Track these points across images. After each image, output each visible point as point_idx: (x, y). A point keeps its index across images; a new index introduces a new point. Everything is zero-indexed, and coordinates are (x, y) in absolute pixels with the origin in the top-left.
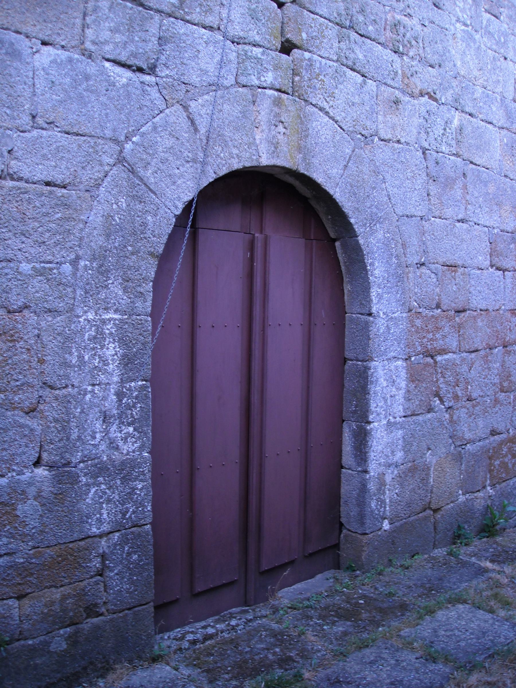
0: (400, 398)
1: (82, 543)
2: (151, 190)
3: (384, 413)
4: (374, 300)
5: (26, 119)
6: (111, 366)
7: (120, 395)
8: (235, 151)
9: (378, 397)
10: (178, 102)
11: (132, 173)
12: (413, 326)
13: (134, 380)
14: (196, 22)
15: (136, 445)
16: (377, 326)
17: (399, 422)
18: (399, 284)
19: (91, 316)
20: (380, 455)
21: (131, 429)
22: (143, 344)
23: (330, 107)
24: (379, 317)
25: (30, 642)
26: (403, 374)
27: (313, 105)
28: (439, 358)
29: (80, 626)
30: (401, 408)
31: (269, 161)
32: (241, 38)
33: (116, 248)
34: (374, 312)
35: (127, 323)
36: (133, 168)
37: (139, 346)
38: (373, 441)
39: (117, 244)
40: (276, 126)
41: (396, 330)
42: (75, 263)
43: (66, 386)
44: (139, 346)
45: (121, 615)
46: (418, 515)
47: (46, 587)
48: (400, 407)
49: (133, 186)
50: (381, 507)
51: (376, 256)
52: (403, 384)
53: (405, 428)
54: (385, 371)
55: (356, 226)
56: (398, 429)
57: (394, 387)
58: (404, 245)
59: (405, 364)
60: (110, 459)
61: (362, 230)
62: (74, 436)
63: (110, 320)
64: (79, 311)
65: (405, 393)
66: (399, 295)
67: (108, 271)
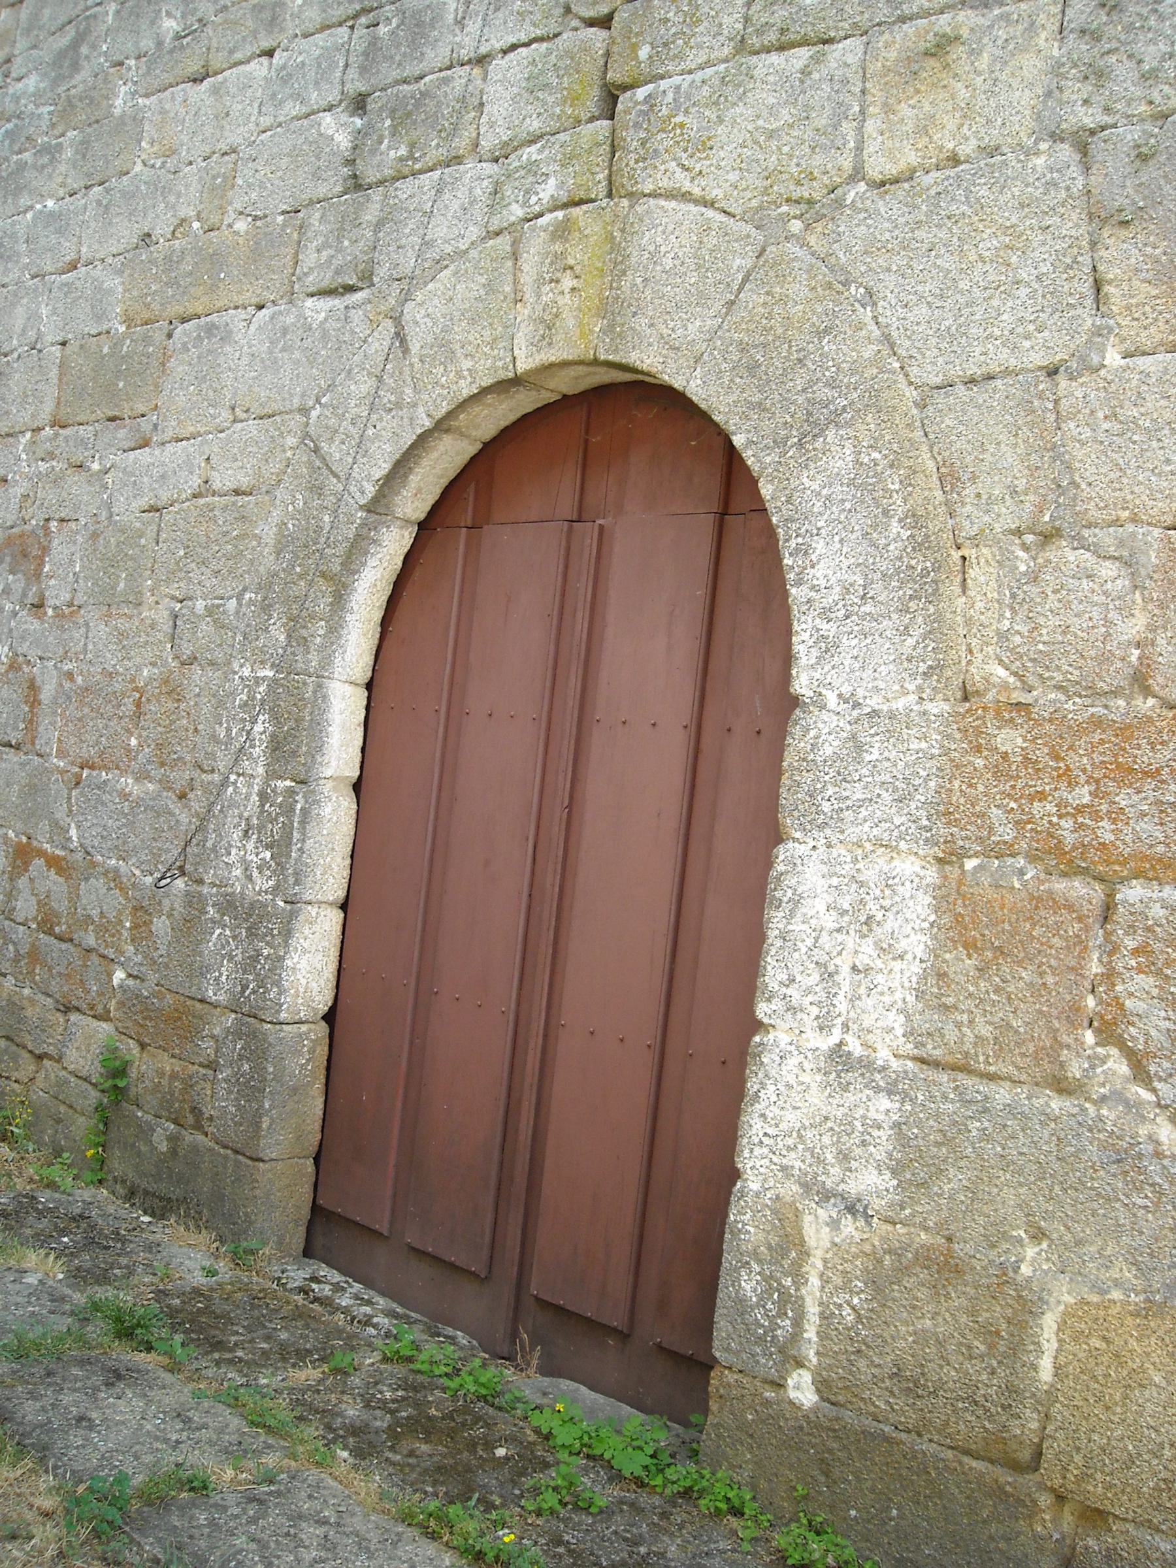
0: (896, 984)
1: (198, 1005)
2: (332, 472)
3: (815, 1011)
4: (802, 655)
5: (226, 414)
6: (257, 749)
7: (263, 796)
8: (467, 364)
9: (796, 955)
10: (386, 316)
11: (315, 452)
12: (978, 749)
13: (280, 778)
14: (300, 257)
15: (270, 883)
16: (812, 733)
17: (884, 1069)
18: (913, 605)
19: (246, 672)
20: (790, 1142)
21: (268, 855)
22: (296, 721)
23: (692, 180)
24: (823, 707)
25: (140, 1114)
26: (920, 907)
27: (649, 195)
28: (1133, 893)
29: (184, 1132)
30: (898, 1022)
31: (530, 360)
32: (506, 144)
33: (284, 570)
34: (803, 691)
35: (282, 685)
36: (315, 445)
37: (292, 724)
38: (763, 1085)
39: (284, 565)
40: (557, 281)
41: (893, 755)
42: (240, 597)
43: (213, 771)
44: (292, 724)
45: (222, 1151)
46: (966, 1459)
47: (224, 1403)
48: (892, 1015)
49: (313, 469)
50: (782, 1314)
51: (820, 524)
52: (916, 944)
53: (905, 1097)
54: (835, 881)
55: (750, 453)
56: (878, 1090)
57: (870, 940)
58: (949, 479)
59: (932, 875)
60: (242, 893)
61: (768, 459)
62: (209, 844)
63: (264, 679)
64: (236, 666)
65: (924, 977)
66: (910, 641)
67: (270, 605)
